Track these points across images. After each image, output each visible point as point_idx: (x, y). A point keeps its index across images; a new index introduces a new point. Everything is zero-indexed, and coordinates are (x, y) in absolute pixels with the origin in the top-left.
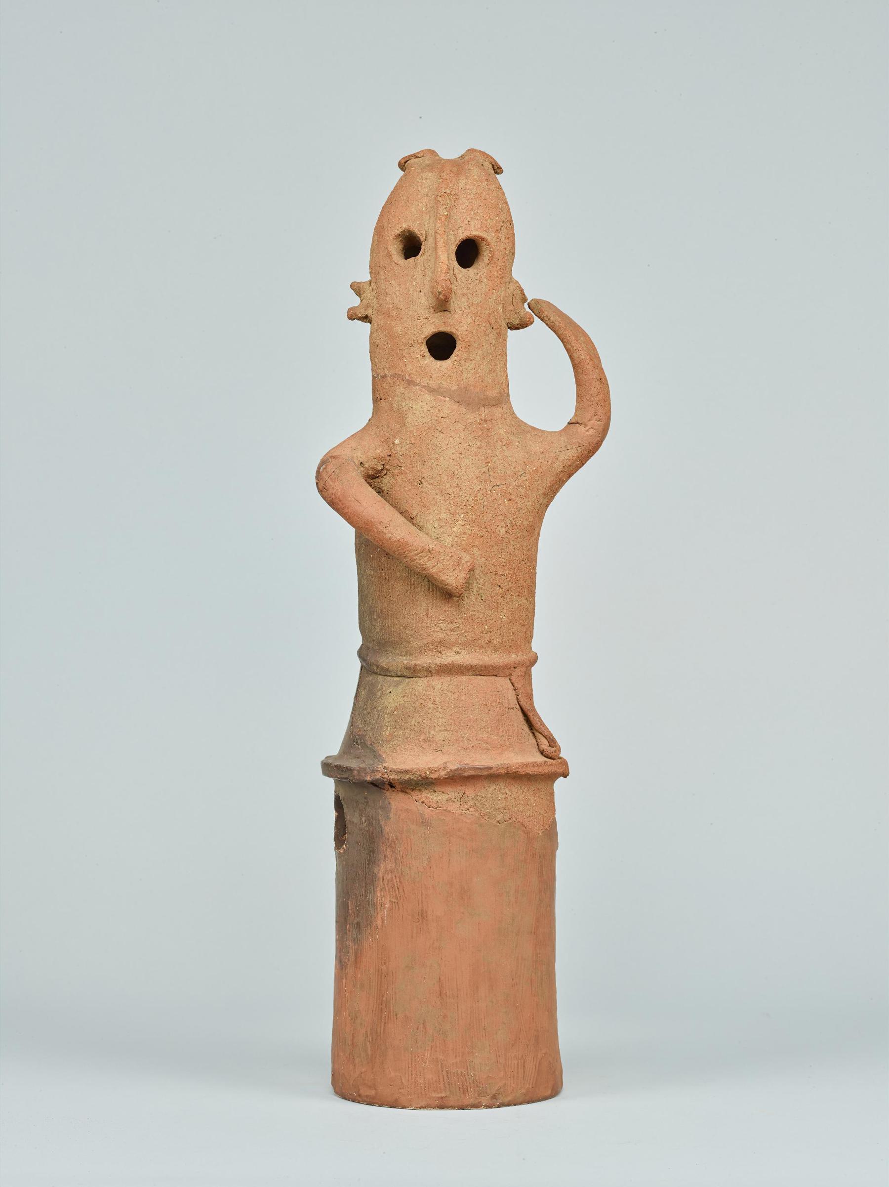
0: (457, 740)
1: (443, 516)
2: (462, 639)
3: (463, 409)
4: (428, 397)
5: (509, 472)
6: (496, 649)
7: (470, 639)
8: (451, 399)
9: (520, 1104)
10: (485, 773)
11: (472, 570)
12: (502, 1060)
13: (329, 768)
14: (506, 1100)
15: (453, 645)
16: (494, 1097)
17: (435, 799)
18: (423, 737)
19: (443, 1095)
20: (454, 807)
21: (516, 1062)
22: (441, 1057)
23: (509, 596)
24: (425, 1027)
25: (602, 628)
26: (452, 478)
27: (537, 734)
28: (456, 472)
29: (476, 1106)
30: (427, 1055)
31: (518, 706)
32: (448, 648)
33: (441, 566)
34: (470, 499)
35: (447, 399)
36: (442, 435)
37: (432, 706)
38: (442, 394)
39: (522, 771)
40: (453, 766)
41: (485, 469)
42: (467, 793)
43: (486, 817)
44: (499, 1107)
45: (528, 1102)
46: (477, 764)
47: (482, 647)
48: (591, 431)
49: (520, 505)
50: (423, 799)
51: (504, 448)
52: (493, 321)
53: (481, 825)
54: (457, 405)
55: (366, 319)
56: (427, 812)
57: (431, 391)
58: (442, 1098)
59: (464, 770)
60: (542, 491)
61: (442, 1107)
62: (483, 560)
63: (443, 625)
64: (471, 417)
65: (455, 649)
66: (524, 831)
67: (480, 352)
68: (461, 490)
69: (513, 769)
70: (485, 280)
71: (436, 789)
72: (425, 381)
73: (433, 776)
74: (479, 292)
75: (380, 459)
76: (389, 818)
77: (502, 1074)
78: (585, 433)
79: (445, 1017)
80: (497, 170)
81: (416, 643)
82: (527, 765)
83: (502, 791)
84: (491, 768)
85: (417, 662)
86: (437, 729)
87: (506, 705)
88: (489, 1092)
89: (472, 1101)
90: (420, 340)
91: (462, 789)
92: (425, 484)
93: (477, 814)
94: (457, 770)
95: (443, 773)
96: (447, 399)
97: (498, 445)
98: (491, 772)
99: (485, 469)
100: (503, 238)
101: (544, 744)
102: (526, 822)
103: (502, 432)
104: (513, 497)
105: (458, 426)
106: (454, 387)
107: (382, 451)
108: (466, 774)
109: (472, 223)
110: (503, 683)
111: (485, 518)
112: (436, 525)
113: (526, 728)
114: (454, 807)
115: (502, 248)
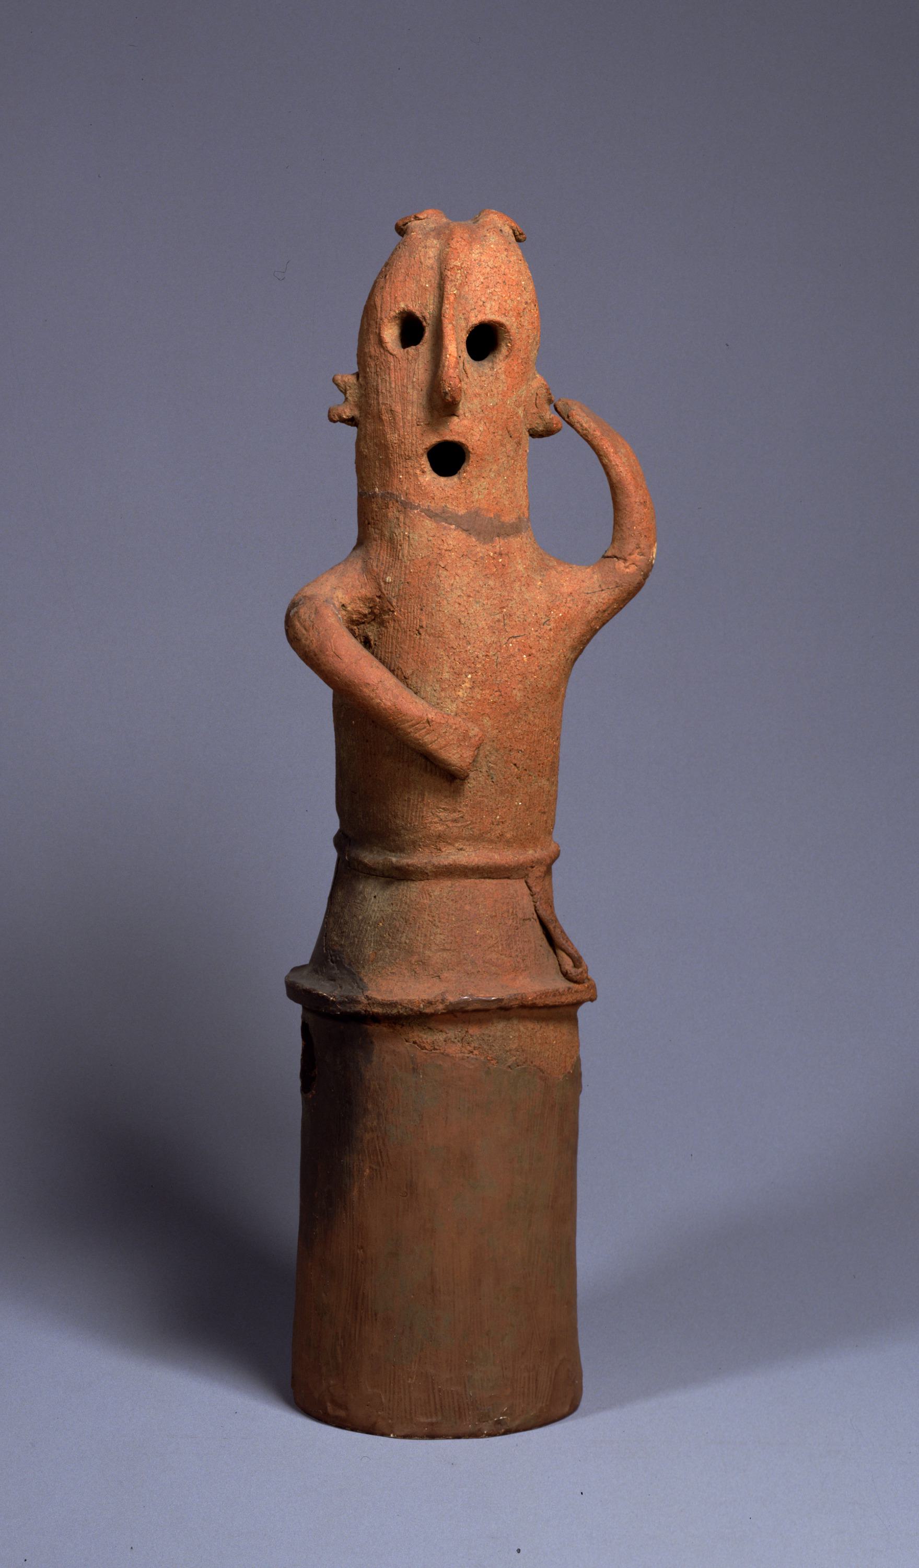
0: (459, 963)
2: (466, 833)
4: (428, 523)
6: (509, 844)
8: (458, 526)
13: (294, 992)
15: (456, 839)
19: (434, 1420)
20: (454, 1050)
28: (463, 620)
34: (480, 656)
35: (453, 527)
38: (446, 520)
40: (451, 998)
44: (505, 1433)
47: (491, 841)
48: (633, 568)
54: (464, 535)
57: (431, 515)
60: (569, 642)
61: (432, 1436)
62: (495, 732)
63: (442, 815)
64: (481, 550)
66: (541, 1078)
67: (495, 467)
72: (426, 504)
73: (427, 1011)
74: (495, 391)
84: (502, 1000)
97: (517, 585)
101: (568, 964)
104: (533, 651)
108: (469, 1008)
109: (488, 305)
110: (517, 887)
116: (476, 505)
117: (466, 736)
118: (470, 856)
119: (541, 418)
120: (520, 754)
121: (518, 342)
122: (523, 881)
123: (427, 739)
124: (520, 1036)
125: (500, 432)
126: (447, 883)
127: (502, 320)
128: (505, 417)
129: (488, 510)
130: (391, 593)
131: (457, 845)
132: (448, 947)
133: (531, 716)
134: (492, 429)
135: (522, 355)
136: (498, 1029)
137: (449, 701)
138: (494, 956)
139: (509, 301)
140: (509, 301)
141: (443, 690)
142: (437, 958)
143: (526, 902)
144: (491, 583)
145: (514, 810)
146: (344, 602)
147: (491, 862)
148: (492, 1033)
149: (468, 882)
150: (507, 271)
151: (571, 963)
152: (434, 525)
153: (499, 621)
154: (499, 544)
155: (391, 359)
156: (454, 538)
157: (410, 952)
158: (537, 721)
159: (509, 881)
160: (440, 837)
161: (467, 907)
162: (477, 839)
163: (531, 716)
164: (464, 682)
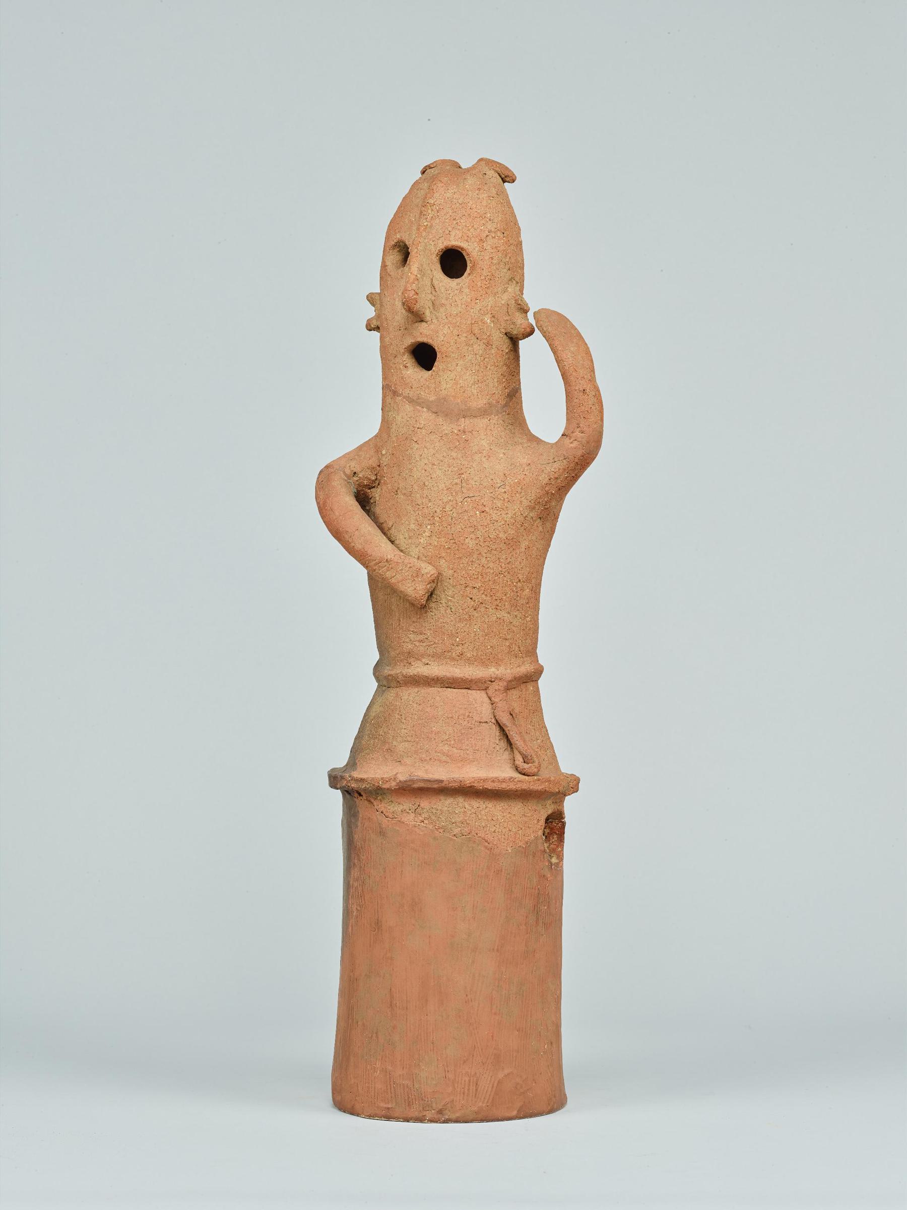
0: (416, 752)
1: (412, 526)
2: (430, 651)
3: (440, 420)
4: (408, 407)
5: (485, 484)
6: (469, 661)
7: (439, 651)
8: (429, 409)
9: (471, 1121)
10: (435, 786)
11: (437, 580)
12: (451, 1076)
13: (335, 779)
14: (453, 1116)
15: (423, 656)
16: (440, 1112)
17: (392, 809)
18: (387, 746)
19: (390, 1106)
20: (409, 819)
21: (467, 1079)
22: (390, 1068)
23: (483, 609)
24: (377, 1037)
25: (610, 649)
26: (422, 489)
27: (515, 751)
28: (427, 483)
29: (420, 1120)
30: (378, 1065)
31: (493, 720)
32: (418, 659)
33: (399, 577)
34: (438, 511)
35: (425, 409)
36: (417, 446)
37: (397, 716)
38: (419, 404)
39: (479, 786)
40: (402, 778)
41: (458, 481)
42: (422, 805)
43: (441, 831)
44: (444, 1122)
45: (482, 1121)
46: (430, 776)
47: (453, 659)
48: (575, 444)
49: (495, 517)
50: (383, 809)
51: (484, 459)
52: (476, 331)
53: (435, 838)
54: (434, 416)
55: (377, 329)
56: (385, 821)
57: (411, 401)
58: (388, 1108)
59: (412, 781)
60: (526, 503)
61: (388, 1118)
62: (451, 572)
63: (412, 636)
64: (447, 427)
65: (425, 660)
66: (486, 847)
67: (461, 362)
68: (430, 501)
69: (468, 783)
70: (466, 290)
71: (393, 799)
72: (407, 392)
73: (384, 786)
74: (459, 302)
75: (372, 469)
76: (357, 827)
77: (450, 1089)
78: (574, 447)
79: (394, 1027)
80: (507, 177)
81: (393, 654)
82: (485, 780)
83: (461, 805)
84: (442, 781)
85: (392, 673)
86: (399, 739)
87: (477, 718)
88: (434, 1105)
89: (416, 1114)
90: (403, 351)
91: (417, 801)
92: (401, 496)
93: (431, 827)
94: (405, 781)
95: (393, 784)
96: (425, 409)
97: (477, 457)
98: (443, 785)
99: (458, 481)
100: (488, 247)
101: (519, 760)
102: (489, 837)
103: (484, 443)
104: (487, 509)
105: (433, 437)
106: (432, 398)
107: (373, 462)
108: (416, 786)
109: (453, 233)
110: (478, 697)
111: (453, 529)
112: (407, 536)
113: (503, 744)
114: (409, 819)
115: (487, 258)
116: (444, 393)
117: (418, 573)
118: (435, 669)
119: (514, 323)
120: (475, 591)
121: (481, 262)
122: (483, 692)
123: (388, 574)
124: (465, 812)
125: (465, 335)
126: (413, 691)
127: (464, 245)
128: (469, 322)
129: (454, 397)
130: (385, 461)
131: (423, 660)
132: (409, 739)
133: (484, 561)
134: (455, 332)
135: (485, 273)
136: (445, 804)
137: (414, 546)
138: (446, 748)
139: (472, 230)
140: (472, 230)
141: (410, 538)
142: (401, 747)
143: (485, 711)
144: (454, 454)
145: (473, 635)
146: (355, 470)
147: (448, 675)
148: (440, 808)
149: (433, 691)
150: (474, 206)
151: (521, 760)
152: (412, 409)
153: (456, 484)
154: (464, 423)
155: (389, 279)
156: (425, 416)
157: (385, 742)
158: (491, 565)
159: (469, 691)
160: (410, 654)
161: (428, 710)
162: (438, 656)
163: (484, 561)
164: (424, 532)
